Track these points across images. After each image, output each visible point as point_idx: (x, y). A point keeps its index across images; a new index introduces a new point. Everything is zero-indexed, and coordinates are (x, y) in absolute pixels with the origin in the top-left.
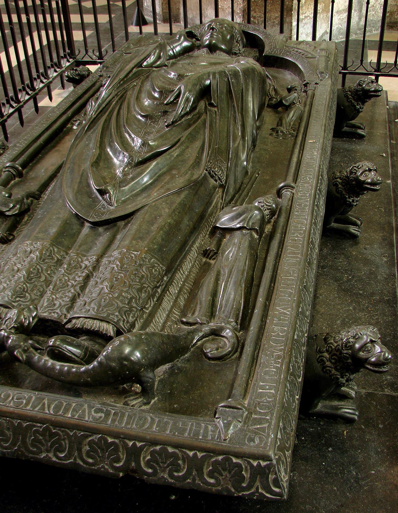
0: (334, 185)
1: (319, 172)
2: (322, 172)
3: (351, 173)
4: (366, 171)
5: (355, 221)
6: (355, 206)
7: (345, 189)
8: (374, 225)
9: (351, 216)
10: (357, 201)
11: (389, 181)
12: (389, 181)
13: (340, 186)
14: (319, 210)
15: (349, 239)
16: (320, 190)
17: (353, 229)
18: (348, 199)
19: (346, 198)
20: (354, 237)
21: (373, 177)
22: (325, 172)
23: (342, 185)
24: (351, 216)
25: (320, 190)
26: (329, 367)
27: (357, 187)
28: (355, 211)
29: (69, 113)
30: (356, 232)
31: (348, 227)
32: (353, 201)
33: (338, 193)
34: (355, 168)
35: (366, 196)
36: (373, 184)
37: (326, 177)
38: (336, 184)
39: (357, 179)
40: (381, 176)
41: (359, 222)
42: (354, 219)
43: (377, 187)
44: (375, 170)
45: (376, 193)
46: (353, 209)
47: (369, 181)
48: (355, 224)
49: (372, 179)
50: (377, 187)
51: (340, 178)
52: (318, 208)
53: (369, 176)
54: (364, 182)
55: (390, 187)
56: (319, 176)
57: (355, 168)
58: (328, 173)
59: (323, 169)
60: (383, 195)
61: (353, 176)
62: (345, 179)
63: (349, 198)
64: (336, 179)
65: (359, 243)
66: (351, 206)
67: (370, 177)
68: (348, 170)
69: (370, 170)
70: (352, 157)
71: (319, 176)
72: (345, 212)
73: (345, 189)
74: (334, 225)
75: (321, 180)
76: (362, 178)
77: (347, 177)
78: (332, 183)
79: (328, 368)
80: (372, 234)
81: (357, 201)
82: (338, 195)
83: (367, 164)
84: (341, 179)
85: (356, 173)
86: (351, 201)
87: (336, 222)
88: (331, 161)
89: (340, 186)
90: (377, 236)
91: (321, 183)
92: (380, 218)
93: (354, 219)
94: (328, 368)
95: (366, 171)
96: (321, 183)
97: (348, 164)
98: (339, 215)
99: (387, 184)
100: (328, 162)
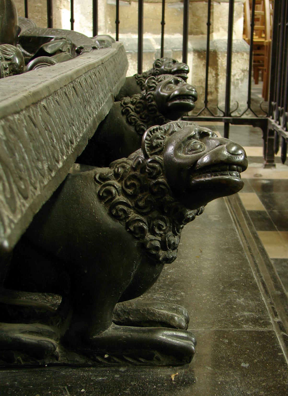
13: (132, 113)
23: (138, 113)
47: (176, 93)
48: (168, 324)
79: (133, 117)
94: (133, 117)
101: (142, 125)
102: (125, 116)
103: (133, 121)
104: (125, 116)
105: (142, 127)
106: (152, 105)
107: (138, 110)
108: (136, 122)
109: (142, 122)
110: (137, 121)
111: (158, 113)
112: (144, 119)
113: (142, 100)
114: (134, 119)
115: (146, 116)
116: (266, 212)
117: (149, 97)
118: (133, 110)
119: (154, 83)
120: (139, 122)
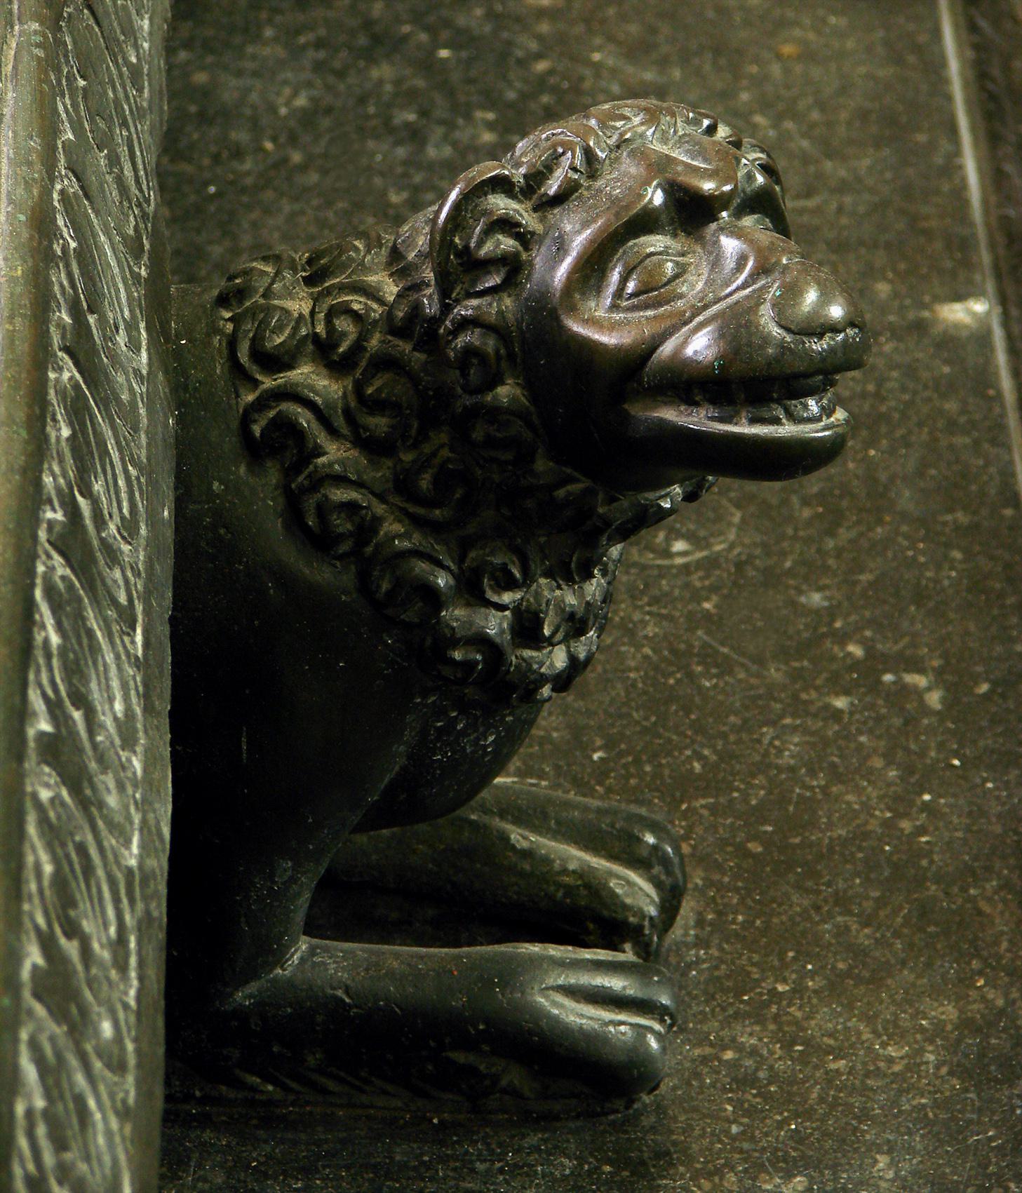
0: (255, 451)
1: (42, 303)
2: (89, 300)
3: (458, 265)
4: (644, 223)
5: (592, 886)
6: (563, 682)
7: (403, 485)
8: (842, 901)
9: (532, 814)
10: (576, 625)
11: (970, 312)
12: (970, 312)
13: (334, 453)
14: (88, 803)
15: (546, 1120)
16: (70, 539)
17: (570, 993)
18: (456, 615)
19: (433, 598)
20: (597, 1083)
21: (737, 289)
22: (121, 299)
23: (371, 446)
24: (532, 814)
25: (70, 539)
26: (340, 480)
27: (565, 444)
28: (578, 740)
29: (113, 496)
30: (620, 1027)
31: (511, 973)
32: (527, 629)
33: (321, 543)
34: (500, 204)
35: (692, 539)
36: (749, 380)
37: (134, 359)
38: (286, 429)
39: (540, 343)
40: (836, 255)
41: (637, 891)
42: (575, 856)
43: (813, 421)
44: (761, 203)
45: (813, 483)
46: (550, 722)
47: (700, 345)
48: (585, 919)
49: (737, 326)
50: (813, 421)
51: (323, 350)
52: (75, 779)
53: (694, 286)
54: (634, 372)
55: (983, 381)
56: (41, 358)
57: (500, 204)
58: (156, 305)
59: (86, 256)
60: (906, 498)
61: (491, 308)
62: (385, 363)
63: (472, 589)
64: (275, 362)
65: (664, 1157)
66: (502, 692)
67: (706, 298)
68: (418, 236)
69: (691, 212)
70: (462, 39)
71: (41, 358)
72: (437, 786)
73: (403, 485)
74: (317, 962)
75: (78, 412)
76: (604, 325)
77: (411, 325)
78: (228, 428)
79: (340, 495)
80: (824, 1021)
81: (576, 625)
82: (323, 574)
83: (646, 140)
84: (337, 366)
85: (513, 268)
86: (495, 624)
87: (350, 907)
88: (191, 136)
89: (334, 453)
90: (895, 1033)
91: (85, 453)
92: (901, 803)
93: (575, 856)
94: (340, 495)
95: (644, 223)
96: (85, 453)
97: (415, 135)
98: (372, 821)
99: (950, 343)
100: (146, 156)
101: (417, 553)
102: (273, 475)
103: (341, 524)
104: (273, 475)
105: (421, 566)
106: (494, 413)
107: (379, 424)
108: (366, 529)
109: (418, 522)
110: (377, 521)
111: (542, 465)
112: (431, 504)
113: (406, 347)
114: (351, 508)
115: (444, 480)
116: (73, 704)
117: (469, 351)
118: (340, 422)
119: (506, 225)
120: (393, 527)
